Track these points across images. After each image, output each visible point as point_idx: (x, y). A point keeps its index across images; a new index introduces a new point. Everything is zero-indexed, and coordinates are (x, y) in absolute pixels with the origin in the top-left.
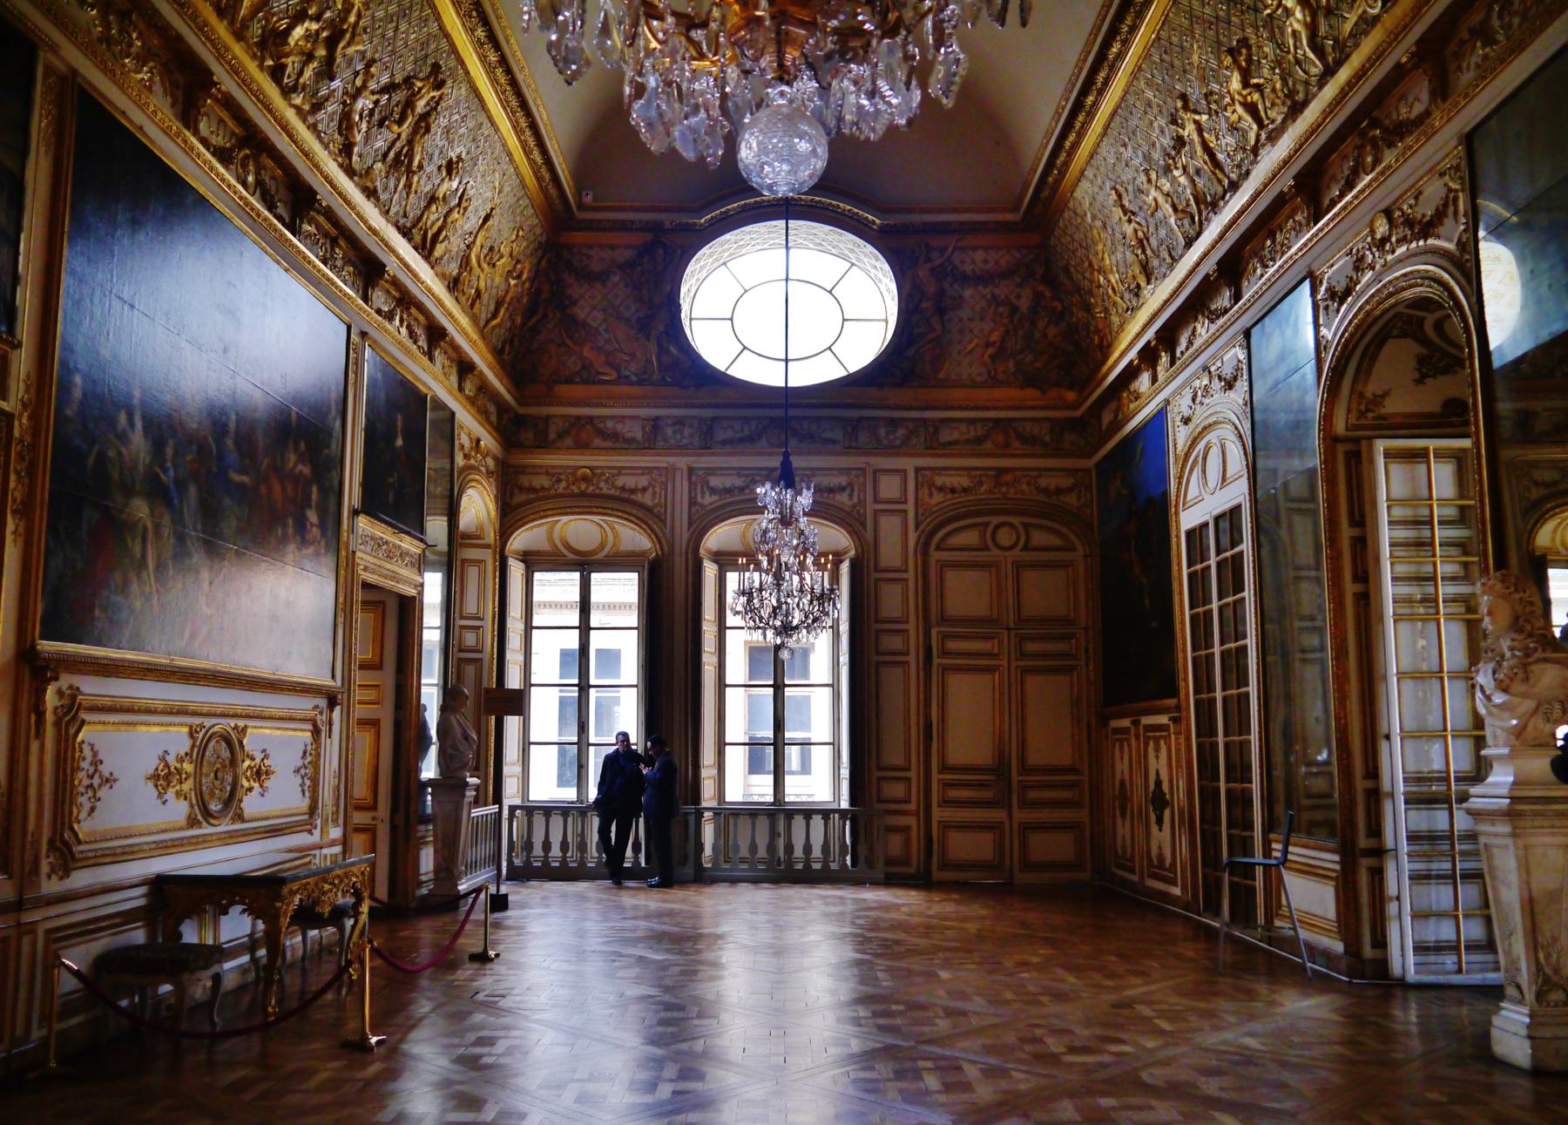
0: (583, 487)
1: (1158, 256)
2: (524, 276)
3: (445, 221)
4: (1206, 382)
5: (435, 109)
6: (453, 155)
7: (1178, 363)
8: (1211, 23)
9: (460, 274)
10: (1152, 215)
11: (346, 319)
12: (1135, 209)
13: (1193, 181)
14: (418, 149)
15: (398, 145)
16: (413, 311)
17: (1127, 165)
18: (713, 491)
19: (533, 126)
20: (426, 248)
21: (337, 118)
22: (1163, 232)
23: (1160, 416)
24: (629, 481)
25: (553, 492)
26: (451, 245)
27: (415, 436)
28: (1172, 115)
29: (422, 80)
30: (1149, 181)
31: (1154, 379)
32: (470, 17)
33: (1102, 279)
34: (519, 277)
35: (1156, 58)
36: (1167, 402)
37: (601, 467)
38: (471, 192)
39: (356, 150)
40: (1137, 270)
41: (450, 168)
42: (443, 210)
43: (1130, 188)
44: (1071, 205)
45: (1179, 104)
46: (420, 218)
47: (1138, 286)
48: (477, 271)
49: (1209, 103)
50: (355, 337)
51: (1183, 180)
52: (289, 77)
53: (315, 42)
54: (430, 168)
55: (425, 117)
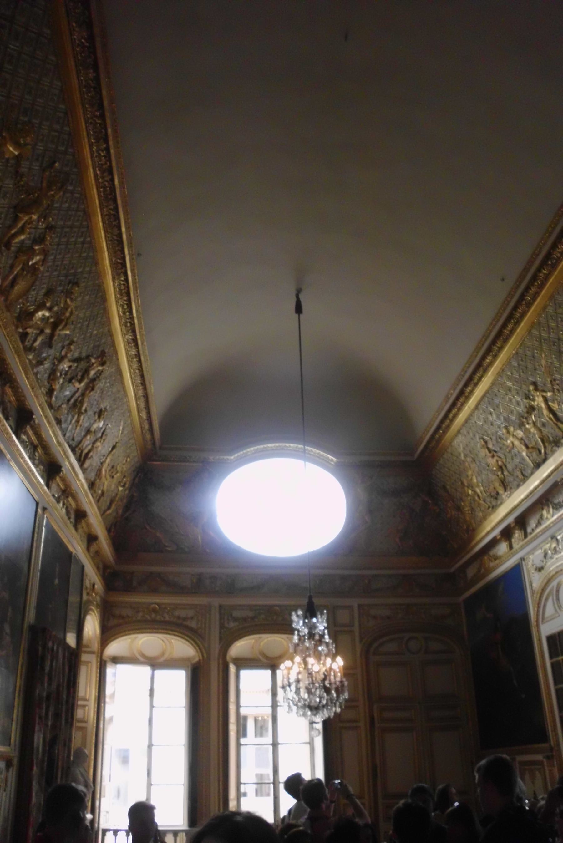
0: (153, 615)
1: (513, 475)
2: (127, 486)
3: (93, 446)
4: (554, 545)
5: (98, 377)
6: (102, 406)
7: (529, 537)
8: (554, 342)
9: (95, 480)
10: (510, 452)
11: (37, 498)
12: (498, 449)
13: (540, 430)
14: (86, 399)
15: (77, 395)
16: (70, 499)
17: (492, 424)
18: (236, 619)
19: (146, 396)
20: (82, 460)
21: (48, 372)
22: (517, 460)
23: (517, 570)
24: (183, 613)
25: (134, 619)
26: (92, 462)
27: (66, 579)
28: (526, 394)
29: (95, 358)
30: (508, 432)
31: (511, 547)
32: (126, 326)
33: (470, 492)
34: (124, 486)
35: (515, 364)
36: (522, 559)
37: (165, 604)
38: (108, 431)
39: (55, 393)
40: (497, 484)
41: (100, 414)
42: (93, 439)
43: (494, 438)
44: (449, 450)
45: (531, 388)
46: (80, 442)
47: (498, 493)
48: (103, 479)
49: (553, 385)
50: (40, 511)
51: (533, 430)
52: (29, 341)
53: (47, 323)
54: (90, 413)
55: (93, 380)
